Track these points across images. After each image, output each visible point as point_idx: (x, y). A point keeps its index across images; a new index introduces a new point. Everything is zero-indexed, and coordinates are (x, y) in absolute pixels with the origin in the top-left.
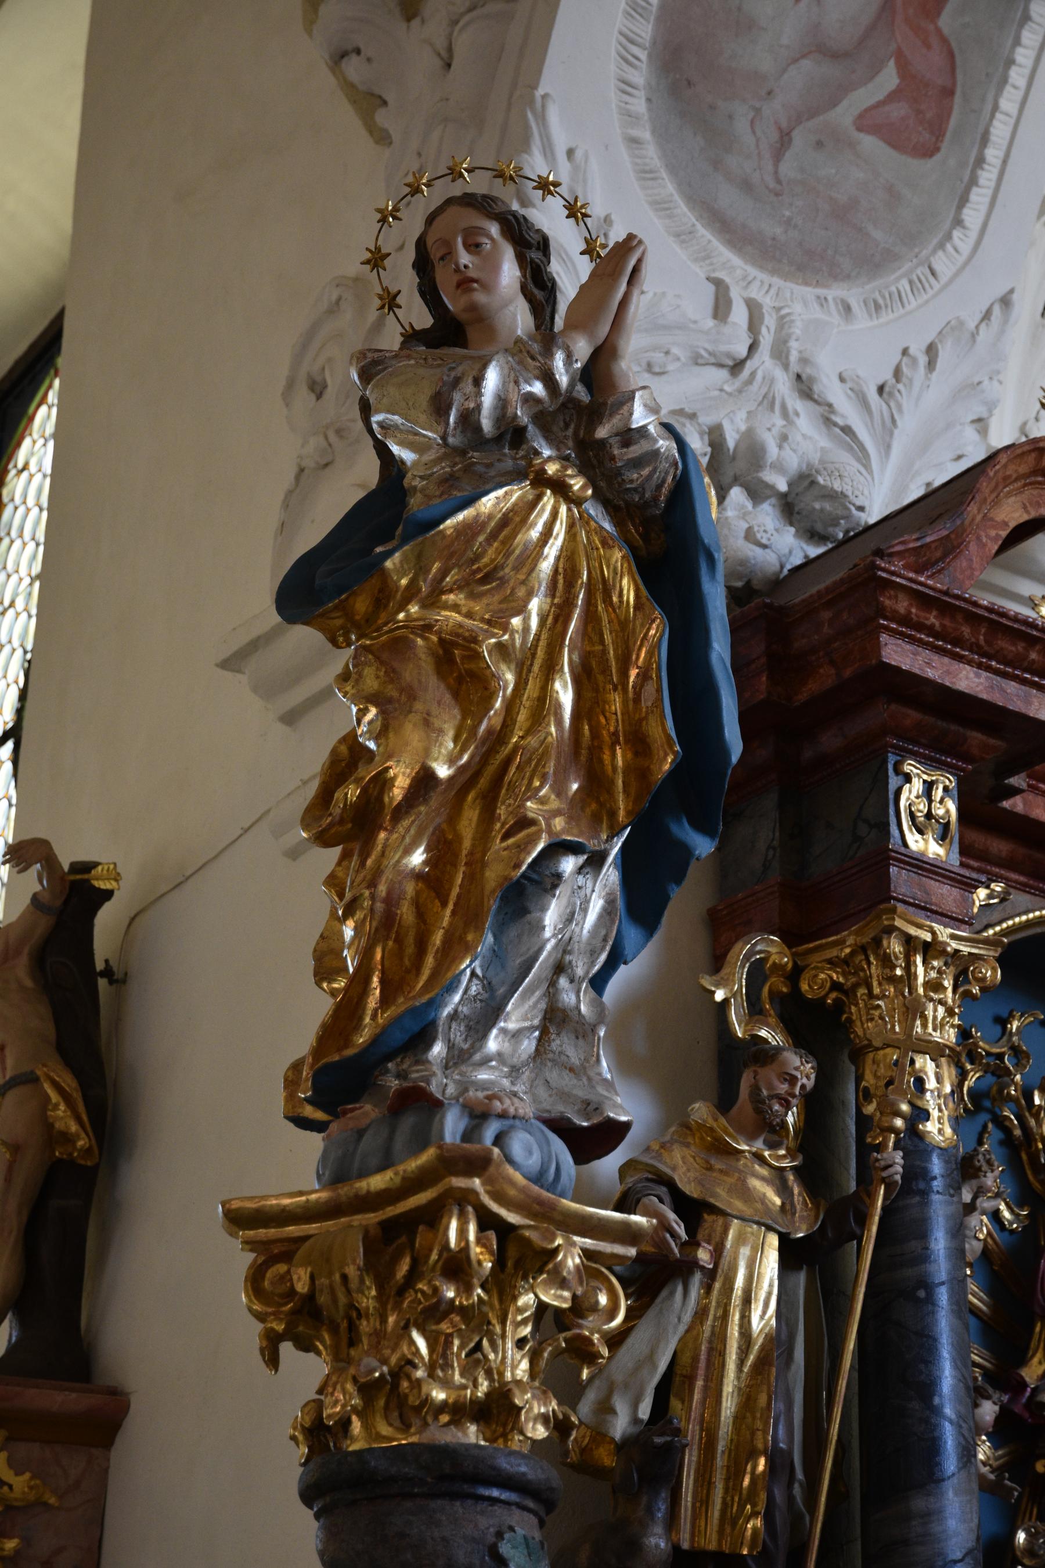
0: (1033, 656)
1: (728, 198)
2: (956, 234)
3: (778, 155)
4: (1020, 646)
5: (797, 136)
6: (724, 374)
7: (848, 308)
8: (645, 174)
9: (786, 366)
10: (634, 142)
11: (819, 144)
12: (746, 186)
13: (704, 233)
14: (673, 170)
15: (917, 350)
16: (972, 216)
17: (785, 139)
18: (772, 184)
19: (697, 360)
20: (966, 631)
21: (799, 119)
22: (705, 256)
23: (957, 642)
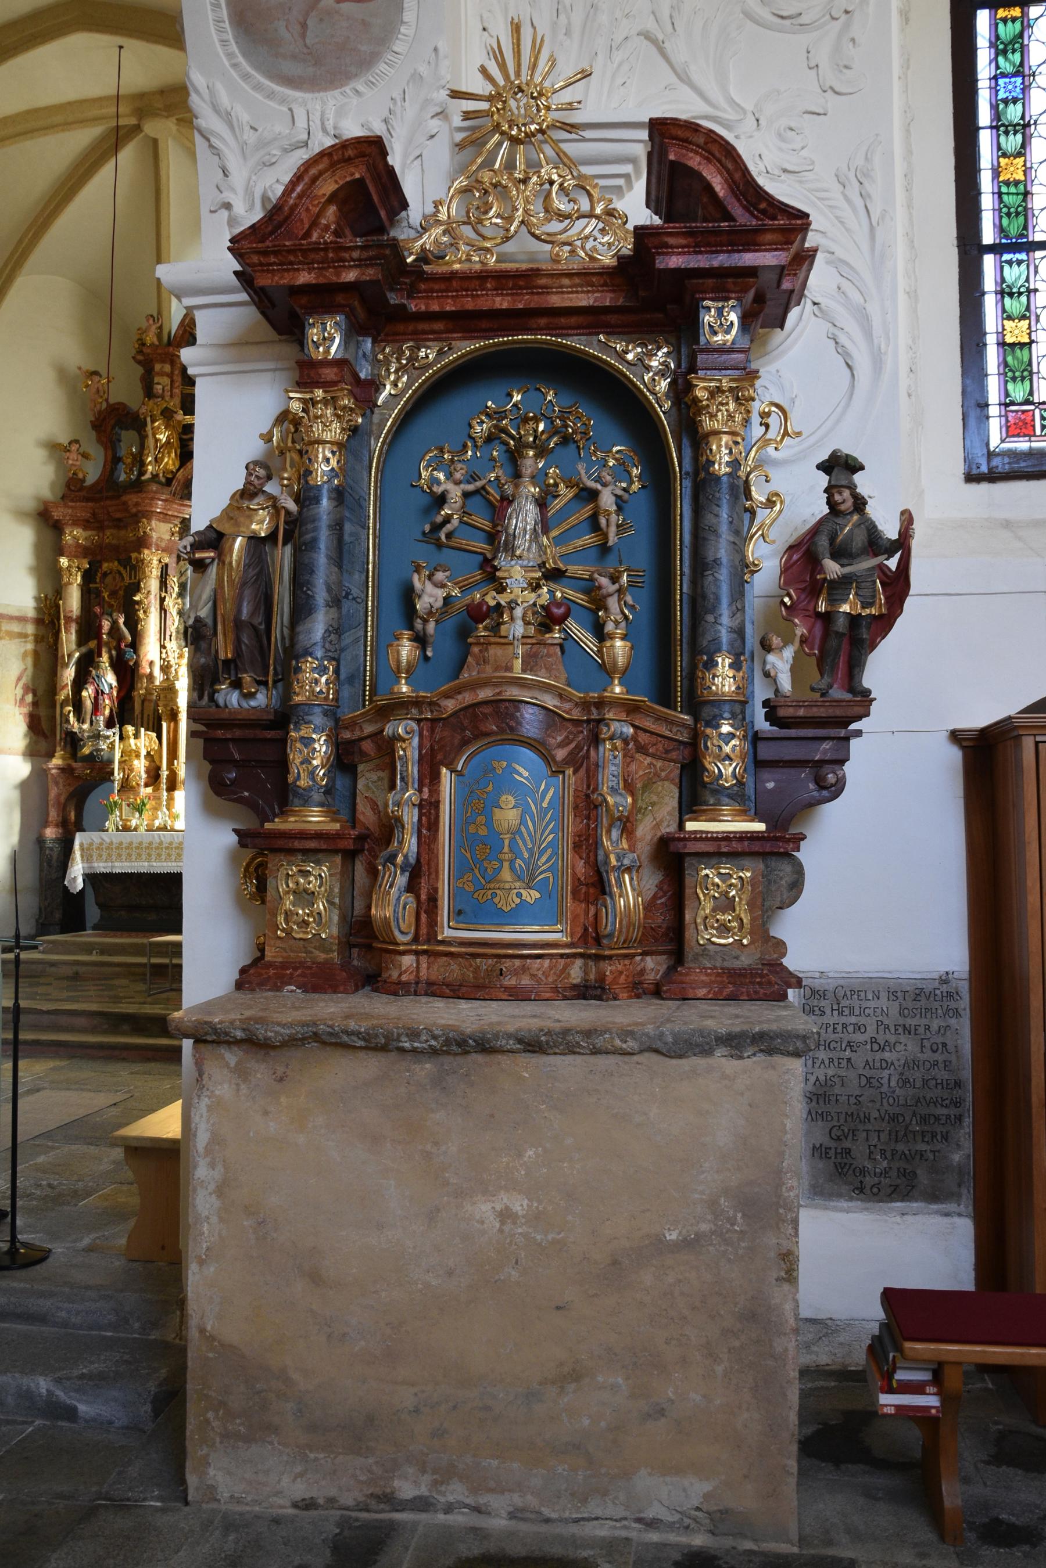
0: (331, 255)
1: (289, 67)
2: (403, 30)
3: (303, 36)
4: (322, 254)
5: (309, 22)
6: (304, 149)
7: (357, 91)
8: (246, 77)
9: (328, 134)
10: (235, 66)
11: (321, 20)
12: (294, 57)
13: (277, 88)
14: (257, 68)
15: (397, 94)
16: (409, 16)
17: (304, 26)
18: (305, 51)
19: (286, 151)
20: (292, 258)
21: (307, 15)
22: (283, 101)
23: (291, 263)
